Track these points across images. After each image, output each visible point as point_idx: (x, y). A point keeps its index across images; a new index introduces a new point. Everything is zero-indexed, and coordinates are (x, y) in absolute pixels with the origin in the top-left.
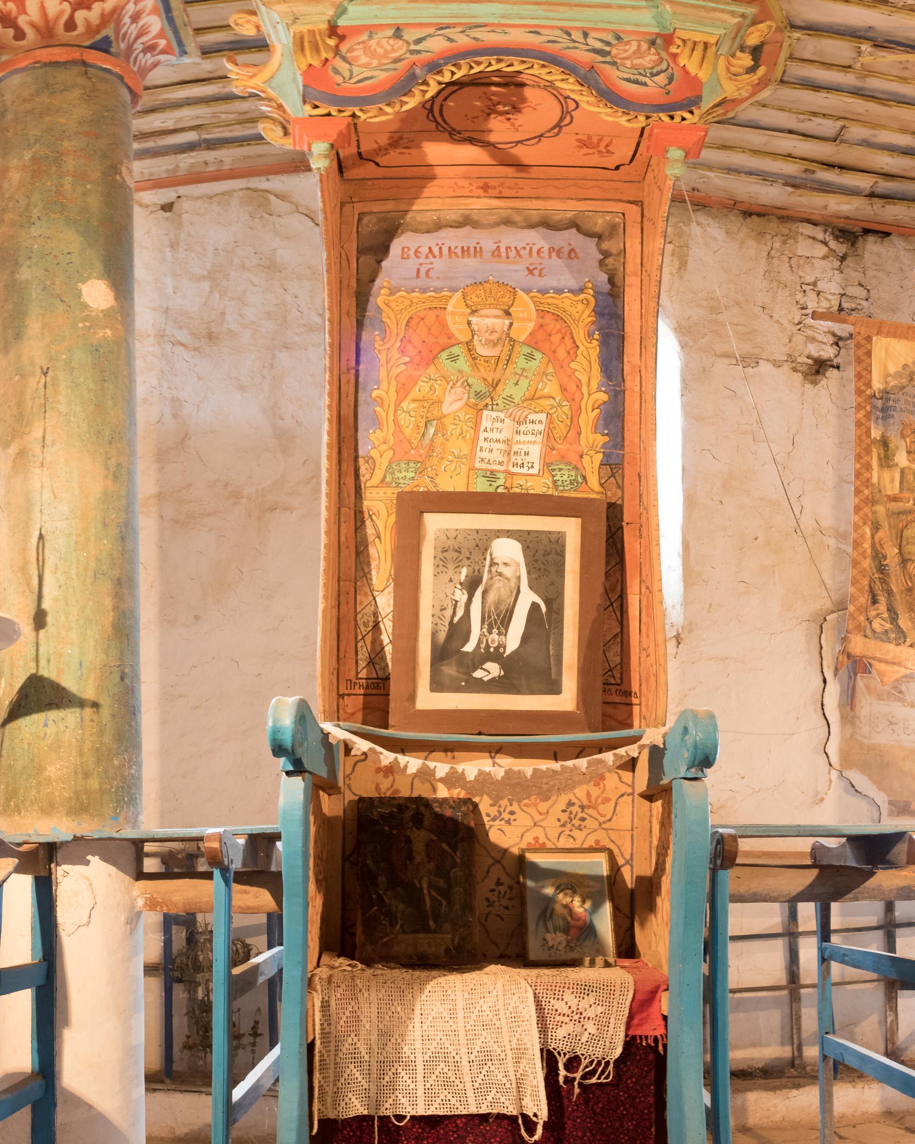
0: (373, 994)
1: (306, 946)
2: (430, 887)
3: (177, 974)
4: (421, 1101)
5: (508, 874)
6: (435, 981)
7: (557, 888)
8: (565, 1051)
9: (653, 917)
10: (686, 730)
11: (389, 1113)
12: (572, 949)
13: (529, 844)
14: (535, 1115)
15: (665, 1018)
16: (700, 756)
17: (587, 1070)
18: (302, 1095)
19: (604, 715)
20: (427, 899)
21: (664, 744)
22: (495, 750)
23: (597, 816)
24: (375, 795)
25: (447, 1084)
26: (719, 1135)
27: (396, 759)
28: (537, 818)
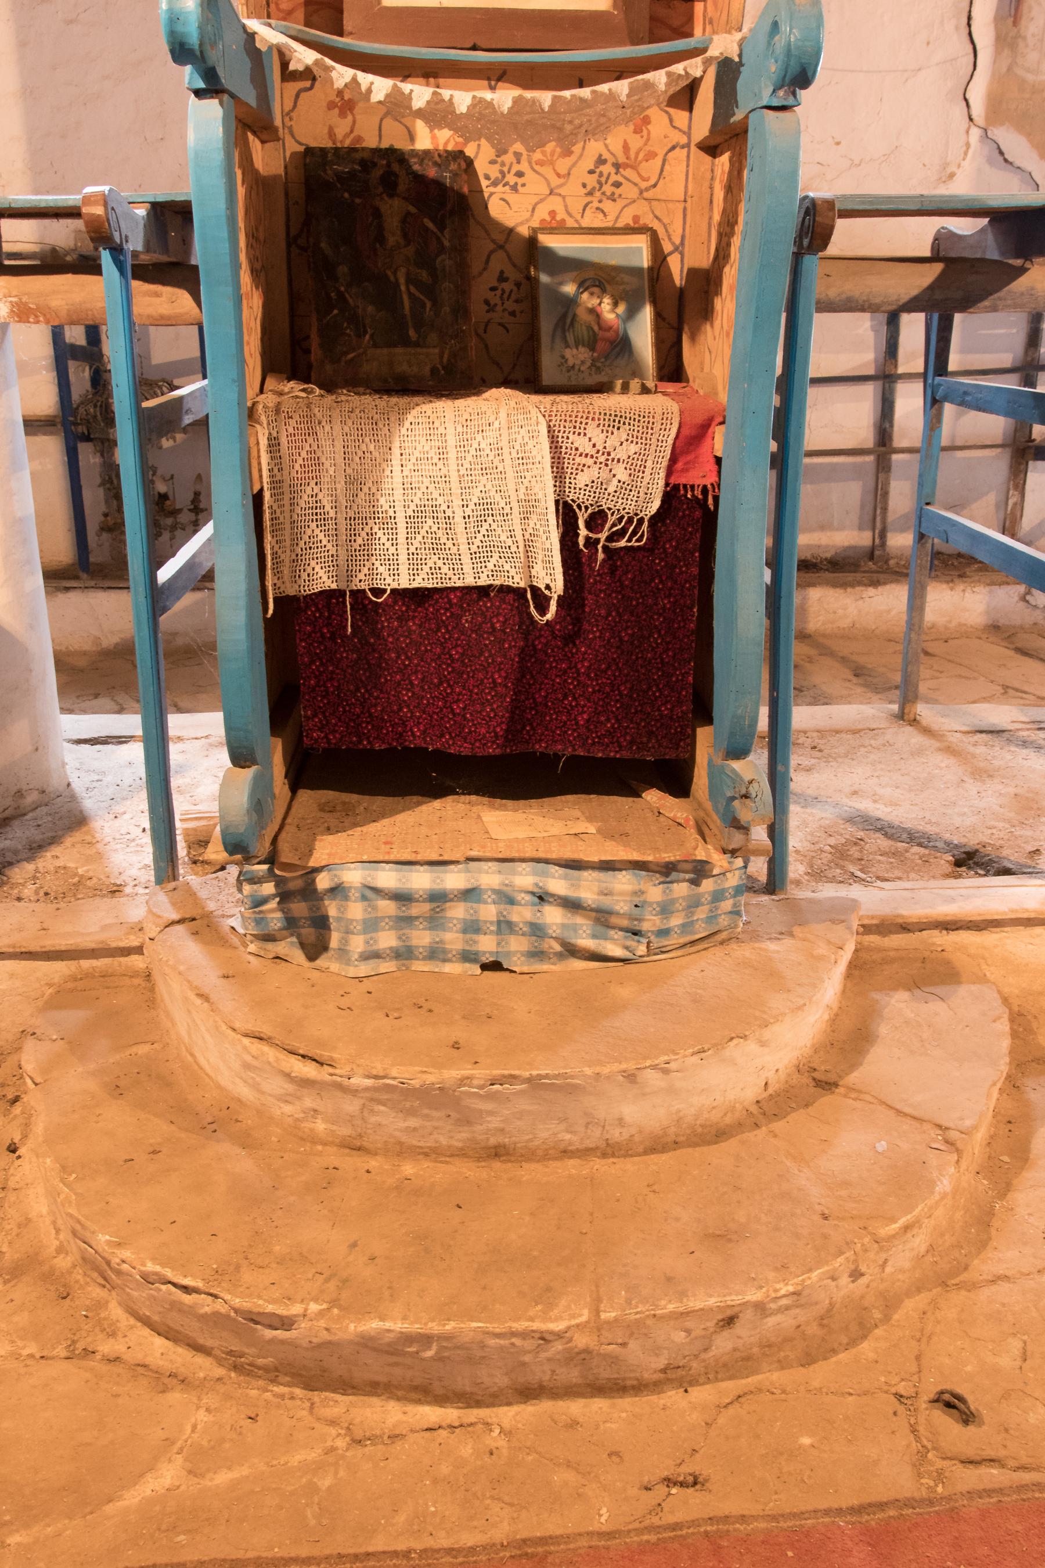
0: (337, 427)
1: (242, 362)
2: (409, 281)
3: (81, 429)
4: (403, 569)
5: (514, 265)
6: (418, 409)
7: (579, 287)
8: (587, 503)
9: (708, 327)
10: (775, 26)
11: (363, 586)
12: (599, 370)
13: (543, 221)
14: (548, 587)
15: (718, 461)
16: (794, 69)
17: (615, 529)
18: (249, 562)
19: (653, 19)
20: (405, 297)
21: (740, 56)
22: (497, 75)
23: (637, 180)
24: (327, 144)
25: (436, 548)
26: (779, 618)
27: (354, 79)
28: (555, 181)
